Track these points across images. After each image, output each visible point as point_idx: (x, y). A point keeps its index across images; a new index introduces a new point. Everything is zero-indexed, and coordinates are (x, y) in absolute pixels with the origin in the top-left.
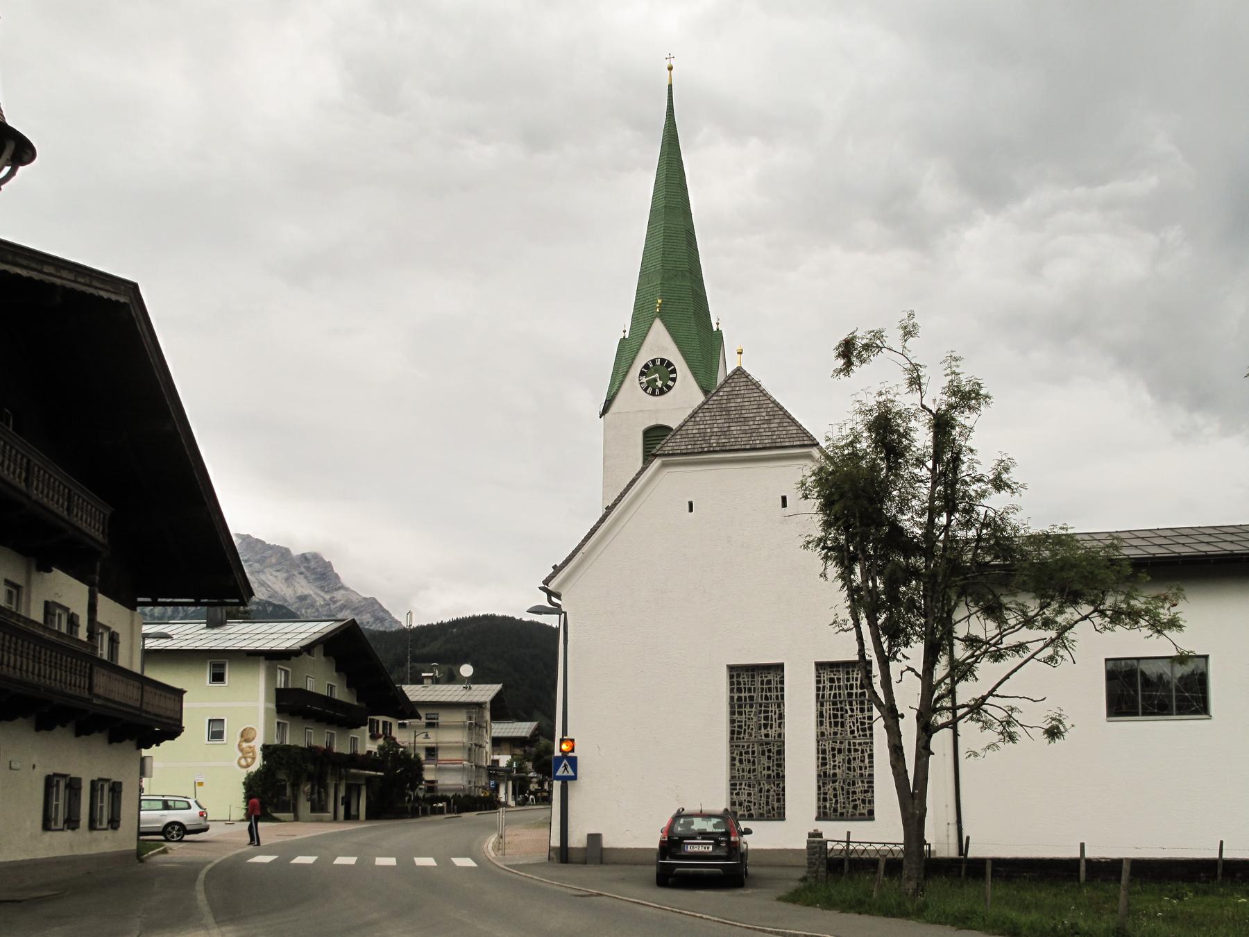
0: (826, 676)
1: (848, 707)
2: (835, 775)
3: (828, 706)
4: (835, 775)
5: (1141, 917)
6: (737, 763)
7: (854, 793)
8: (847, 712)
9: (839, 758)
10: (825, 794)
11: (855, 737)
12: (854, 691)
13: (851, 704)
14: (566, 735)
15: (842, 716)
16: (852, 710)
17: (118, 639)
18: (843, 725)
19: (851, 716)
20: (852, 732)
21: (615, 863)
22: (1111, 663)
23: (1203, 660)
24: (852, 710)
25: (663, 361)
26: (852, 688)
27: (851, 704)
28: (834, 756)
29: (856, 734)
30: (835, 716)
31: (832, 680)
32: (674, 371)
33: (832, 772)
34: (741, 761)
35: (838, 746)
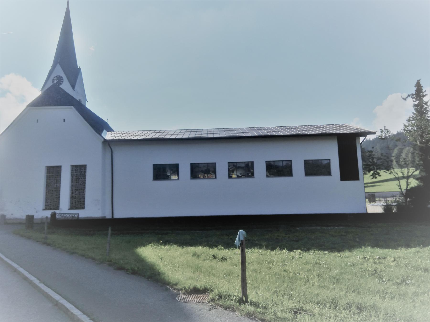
0: (74, 169)
1: (80, 178)
2: (75, 197)
3: (74, 177)
4: (75, 197)
5: (276, 261)
6: (48, 194)
7: (81, 202)
8: (80, 179)
9: (77, 192)
10: (72, 202)
11: (81, 186)
12: (82, 173)
13: (81, 177)
14: (82, 207)
15: (78, 180)
16: (81, 178)
17: (40, 219)
18: (78, 182)
19: (81, 180)
20: (81, 184)
21: (13, 224)
22: (267, 163)
23: (329, 161)
24: (81, 178)
25: (59, 76)
26: (81, 172)
27: (81, 177)
28: (75, 191)
29: (82, 185)
30: (76, 180)
31: (76, 170)
32: (63, 79)
33: (75, 196)
34: (49, 193)
35: (77, 189)
